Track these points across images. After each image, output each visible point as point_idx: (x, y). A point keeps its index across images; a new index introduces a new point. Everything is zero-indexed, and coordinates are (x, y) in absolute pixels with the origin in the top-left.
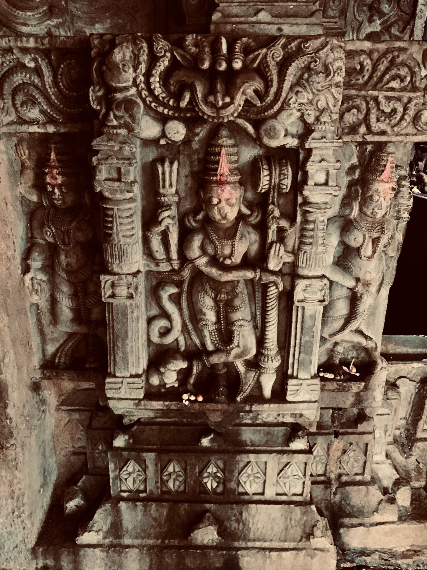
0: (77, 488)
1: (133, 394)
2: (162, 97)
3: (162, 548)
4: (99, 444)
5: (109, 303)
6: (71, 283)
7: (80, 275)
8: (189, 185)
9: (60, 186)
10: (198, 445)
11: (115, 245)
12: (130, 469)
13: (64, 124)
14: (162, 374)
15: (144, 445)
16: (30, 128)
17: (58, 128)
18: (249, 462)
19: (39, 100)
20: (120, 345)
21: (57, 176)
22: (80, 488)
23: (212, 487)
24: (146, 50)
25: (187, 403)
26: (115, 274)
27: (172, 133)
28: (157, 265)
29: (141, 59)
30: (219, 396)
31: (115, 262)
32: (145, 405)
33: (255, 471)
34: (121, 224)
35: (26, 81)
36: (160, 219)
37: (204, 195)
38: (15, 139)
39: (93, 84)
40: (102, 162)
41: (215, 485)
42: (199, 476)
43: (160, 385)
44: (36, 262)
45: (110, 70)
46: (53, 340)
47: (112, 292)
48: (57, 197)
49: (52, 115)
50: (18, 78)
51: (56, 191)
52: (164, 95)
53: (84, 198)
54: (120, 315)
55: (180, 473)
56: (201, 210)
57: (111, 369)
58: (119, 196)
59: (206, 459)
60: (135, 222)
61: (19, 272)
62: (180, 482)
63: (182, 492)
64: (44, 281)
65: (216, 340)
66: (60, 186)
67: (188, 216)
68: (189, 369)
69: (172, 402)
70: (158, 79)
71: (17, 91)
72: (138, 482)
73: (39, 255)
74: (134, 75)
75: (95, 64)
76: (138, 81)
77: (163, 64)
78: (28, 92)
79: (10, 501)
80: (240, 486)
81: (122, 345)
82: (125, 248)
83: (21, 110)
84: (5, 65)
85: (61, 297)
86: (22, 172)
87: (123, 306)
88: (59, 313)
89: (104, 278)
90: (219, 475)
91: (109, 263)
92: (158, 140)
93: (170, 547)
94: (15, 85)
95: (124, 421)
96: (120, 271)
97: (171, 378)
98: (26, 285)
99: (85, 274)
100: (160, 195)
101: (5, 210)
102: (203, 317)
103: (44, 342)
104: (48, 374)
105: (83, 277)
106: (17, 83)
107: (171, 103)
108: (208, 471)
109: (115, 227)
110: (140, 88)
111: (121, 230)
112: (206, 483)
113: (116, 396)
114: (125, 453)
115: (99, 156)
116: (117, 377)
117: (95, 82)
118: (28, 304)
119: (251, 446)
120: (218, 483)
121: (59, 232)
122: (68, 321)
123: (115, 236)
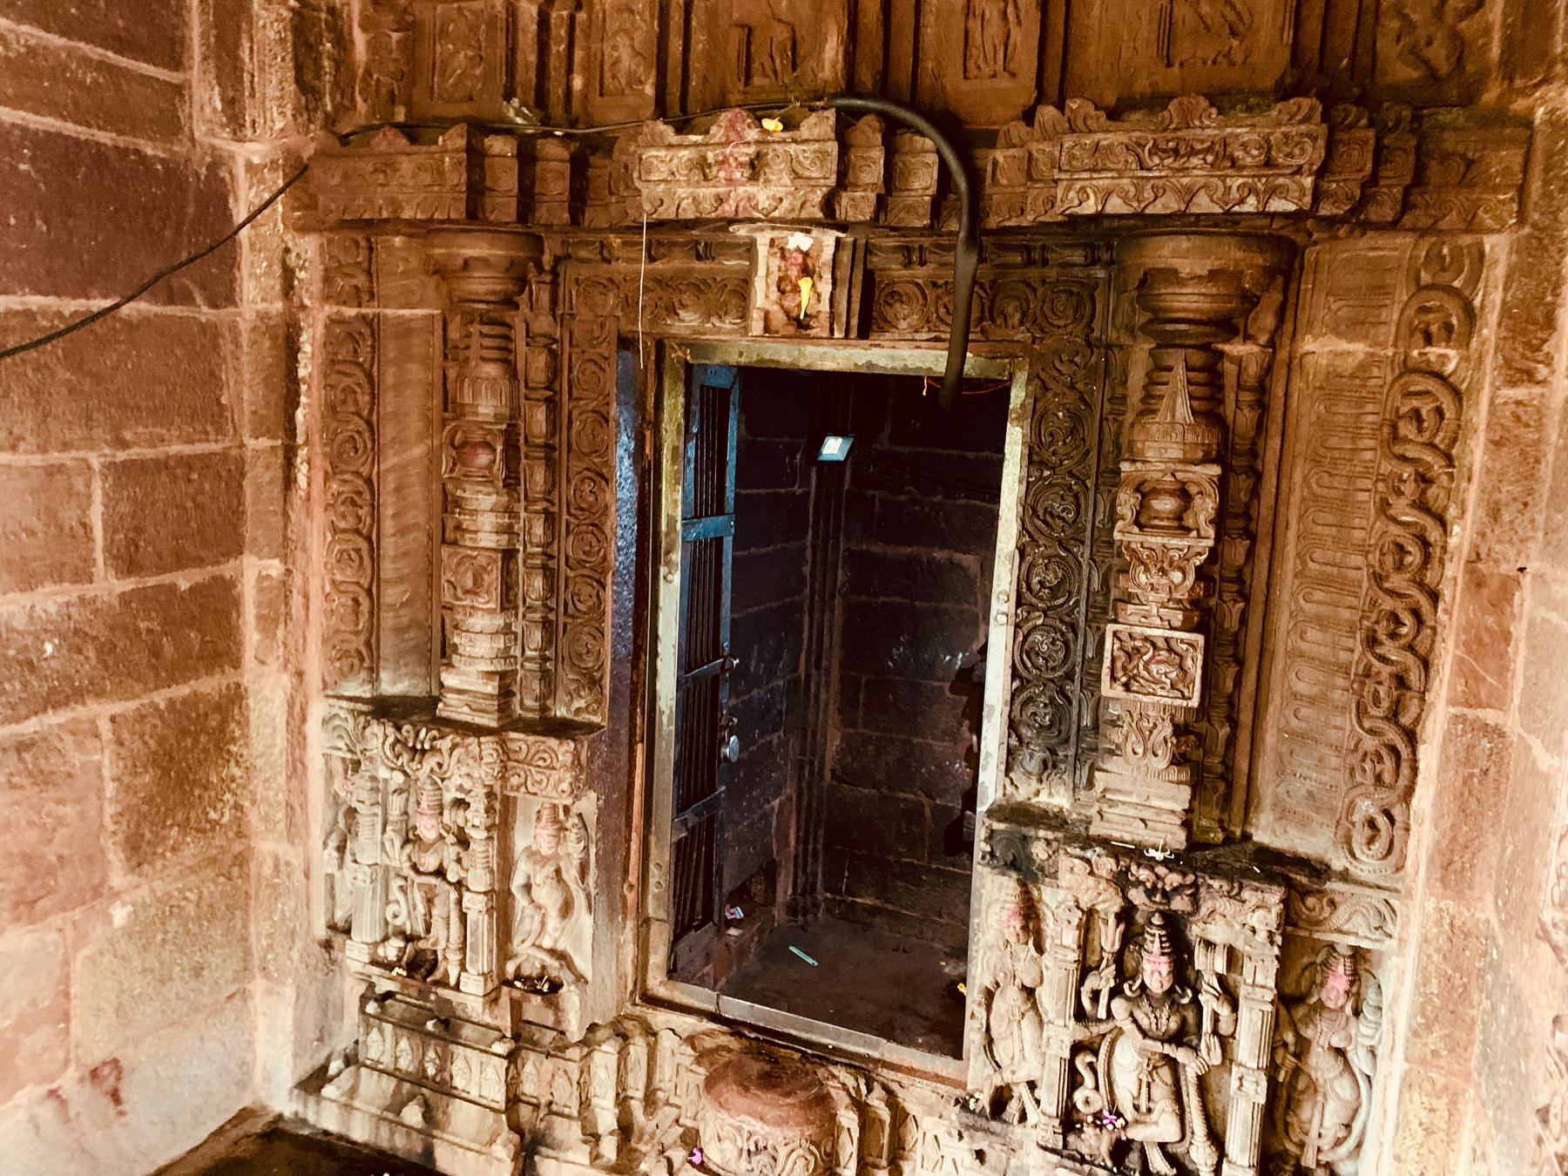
3: (381, 1118)
77: (391, 740)
93: (385, 1119)
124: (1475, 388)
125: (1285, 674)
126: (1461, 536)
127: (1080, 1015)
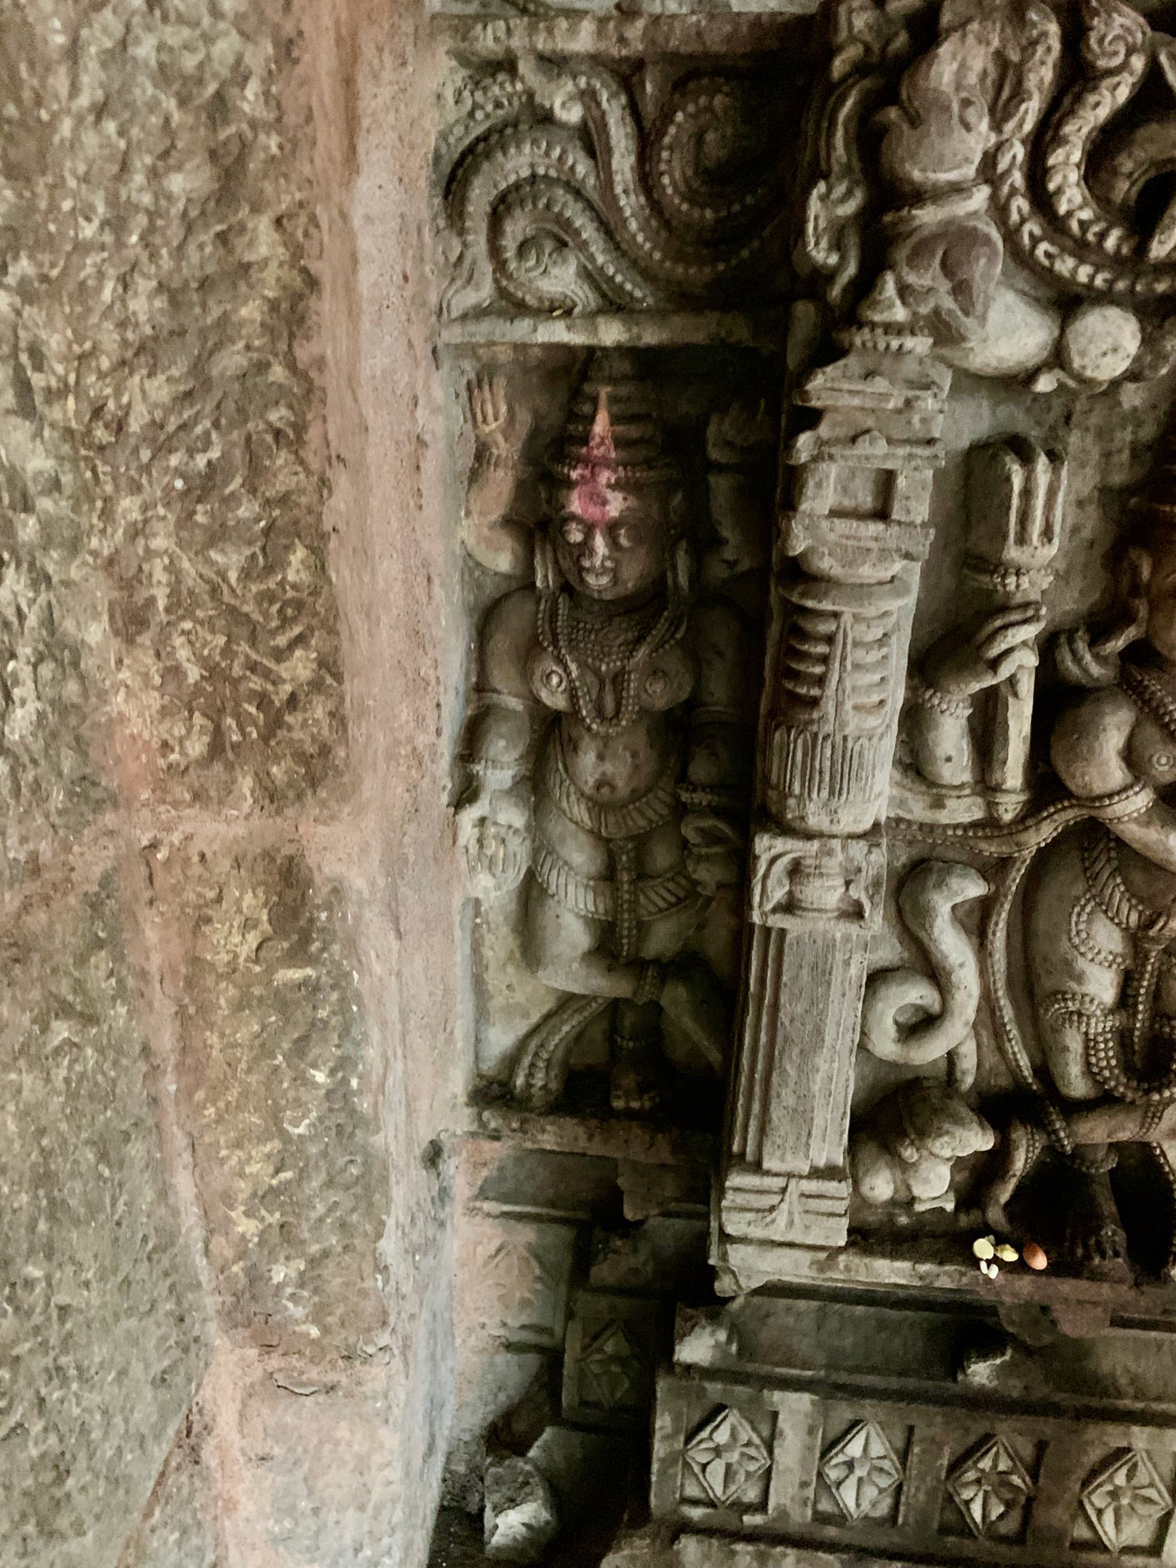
0: (528, 1467)
1: (815, 1231)
2: (1081, 223)
4: (608, 1333)
5: (767, 931)
6: (603, 841)
7: (635, 814)
8: (1086, 533)
9: (612, 529)
10: (955, 1380)
11: (825, 738)
12: (722, 1436)
13: (658, 315)
14: (905, 1166)
15: (777, 1365)
16: (541, 329)
17: (635, 330)
18: (1128, 1450)
19: (584, 236)
20: (791, 1070)
21: (610, 495)
22: (537, 1468)
23: (984, 1517)
24: (1056, 45)
25: (994, 1272)
26: (809, 836)
27: (1094, 351)
28: (938, 803)
29: (1031, 82)
30: (1103, 1256)
31: (814, 795)
32: (847, 1269)
33: (1142, 1477)
34: (857, 666)
35: (541, 171)
36: (994, 652)
37: (1154, 571)
38: (468, 366)
39: (826, 177)
40: (833, 450)
41: (997, 1510)
42: (947, 1477)
43: (893, 1202)
44: (501, 768)
45: (915, 120)
46: (509, 1011)
47: (790, 892)
48: (598, 563)
49: (621, 287)
50: (518, 162)
51: (600, 543)
52: (1086, 214)
53: (674, 568)
54: (805, 972)
55: (886, 1465)
56: (1127, 618)
57: (743, 1141)
58: (867, 572)
59: (979, 1427)
60: (893, 661)
61: (445, 798)
62: (881, 1491)
63: (879, 1522)
64: (516, 831)
65: (1109, 1067)
66: (612, 529)
67: (1071, 641)
69: (941, 1263)
70: (1077, 156)
71: (509, 209)
72: (741, 1477)
73: (506, 748)
74: (993, 139)
75: (850, 103)
76: (1003, 164)
78: (548, 207)
79: (351, 1514)
80: (1080, 1520)
81: (800, 1070)
82: (857, 748)
83: (518, 269)
84: (479, 115)
85: (562, 881)
86: (474, 476)
87: (820, 942)
88: (550, 932)
89: (765, 845)
90: (1016, 1480)
91: (791, 795)
92: (1032, 375)
94: (503, 186)
95: (717, 1285)
96: (826, 826)
97: (934, 1186)
98: (462, 841)
99: (650, 813)
100: (998, 567)
101: (425, 600)
102: (1073, 985)
103: (482, 1016)
104: (493, 1125)
105: (642, 823)
106: (512, 178)
107: (1110, 243)
108: (981, 1465)
109: (836, 677)
110: (1006, 189)
111: (854, 688)
112: (967, 1503)
113: (757, 1232)
114: (714, 1389)
115: (824, 430)
116: (768, 1173)
117: (836, 168)
118: (457, 901)
119: (1136, 1398)
120: (1009, 1505)
121: (590, 678)
122: (572, 960)
123: (829, 707)
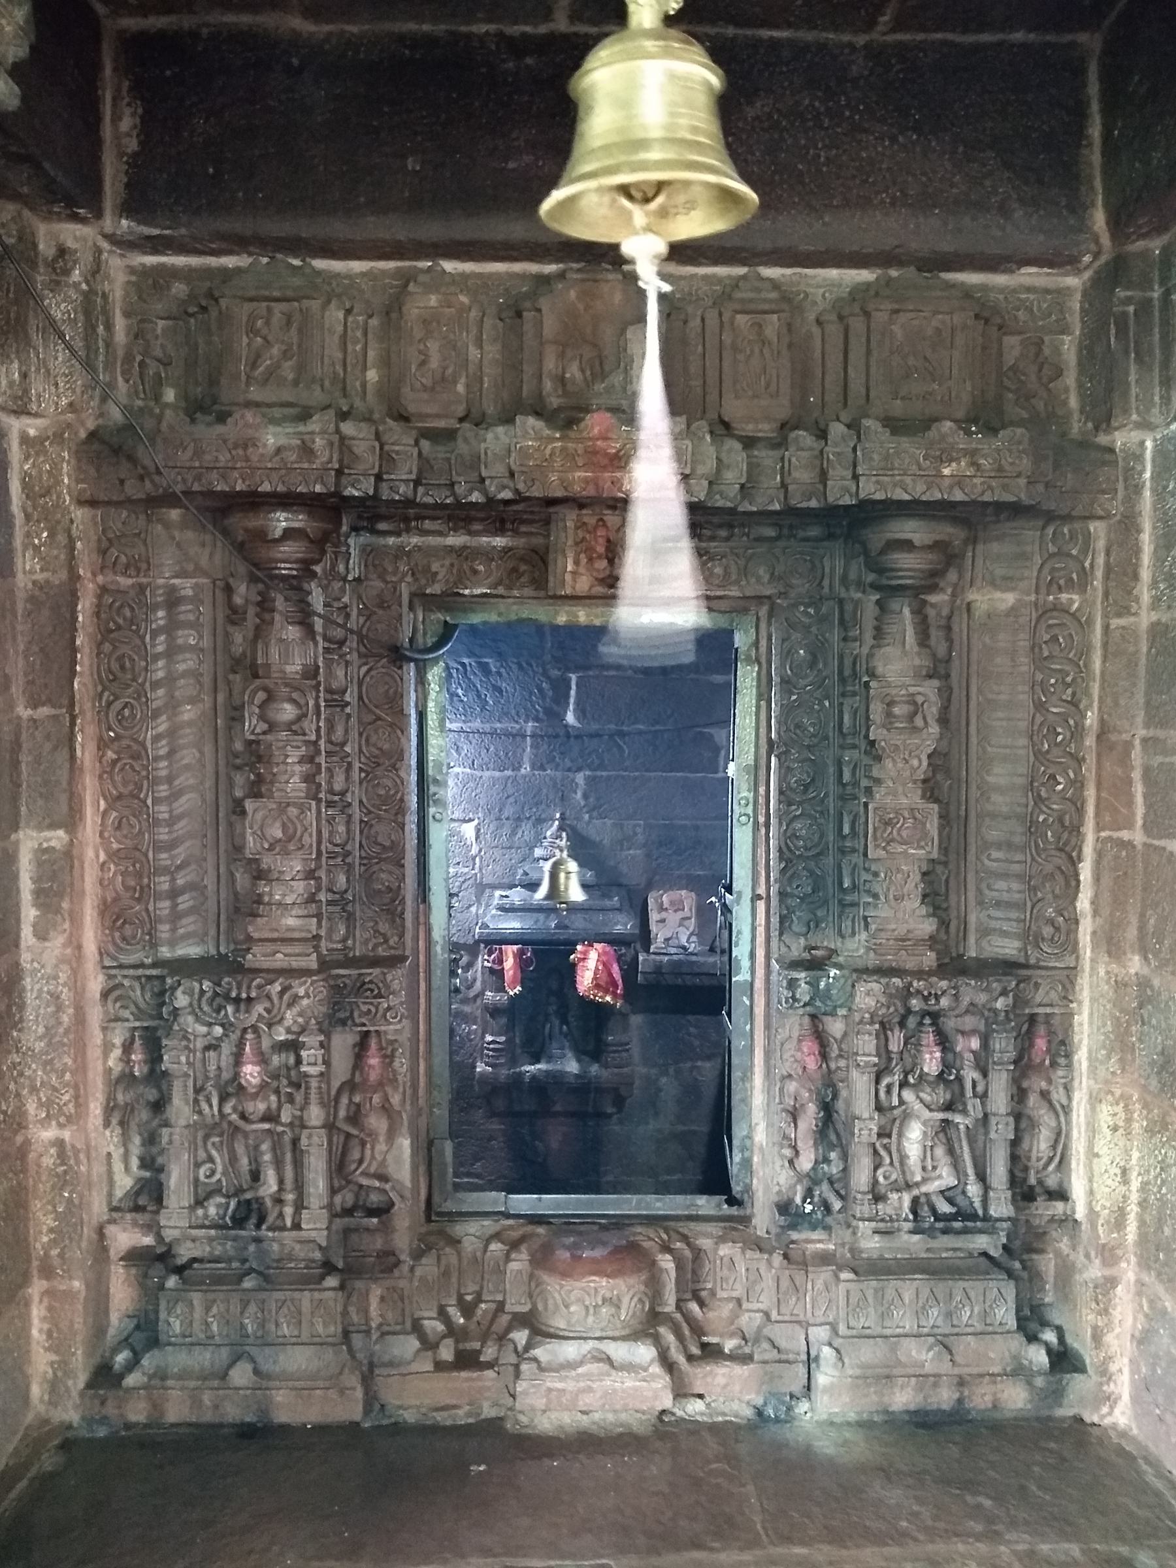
68: (228, 1204)
124: (1090, 622)
125: (978, 828)
126: (1091, 719)
127: (879, 1108)
